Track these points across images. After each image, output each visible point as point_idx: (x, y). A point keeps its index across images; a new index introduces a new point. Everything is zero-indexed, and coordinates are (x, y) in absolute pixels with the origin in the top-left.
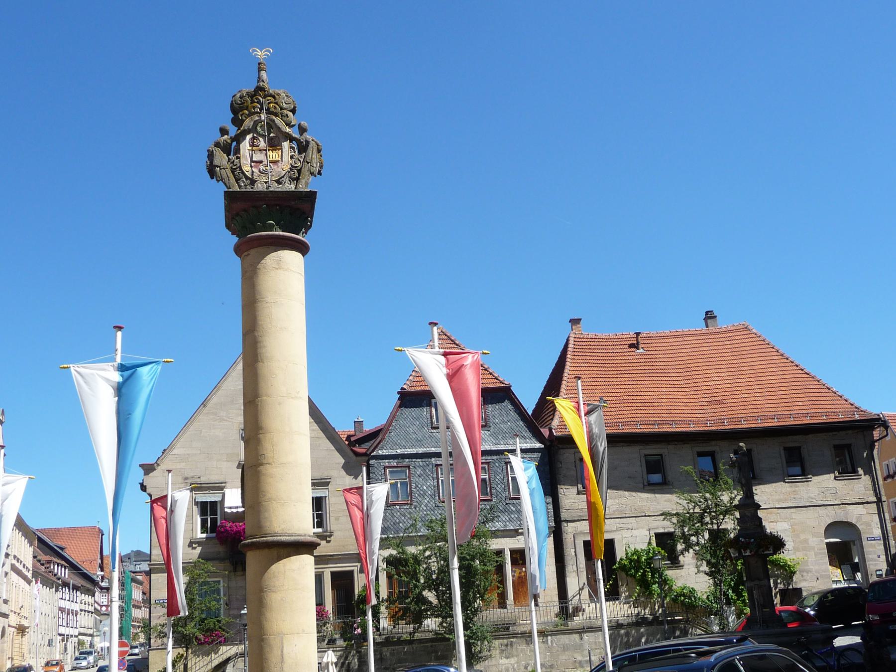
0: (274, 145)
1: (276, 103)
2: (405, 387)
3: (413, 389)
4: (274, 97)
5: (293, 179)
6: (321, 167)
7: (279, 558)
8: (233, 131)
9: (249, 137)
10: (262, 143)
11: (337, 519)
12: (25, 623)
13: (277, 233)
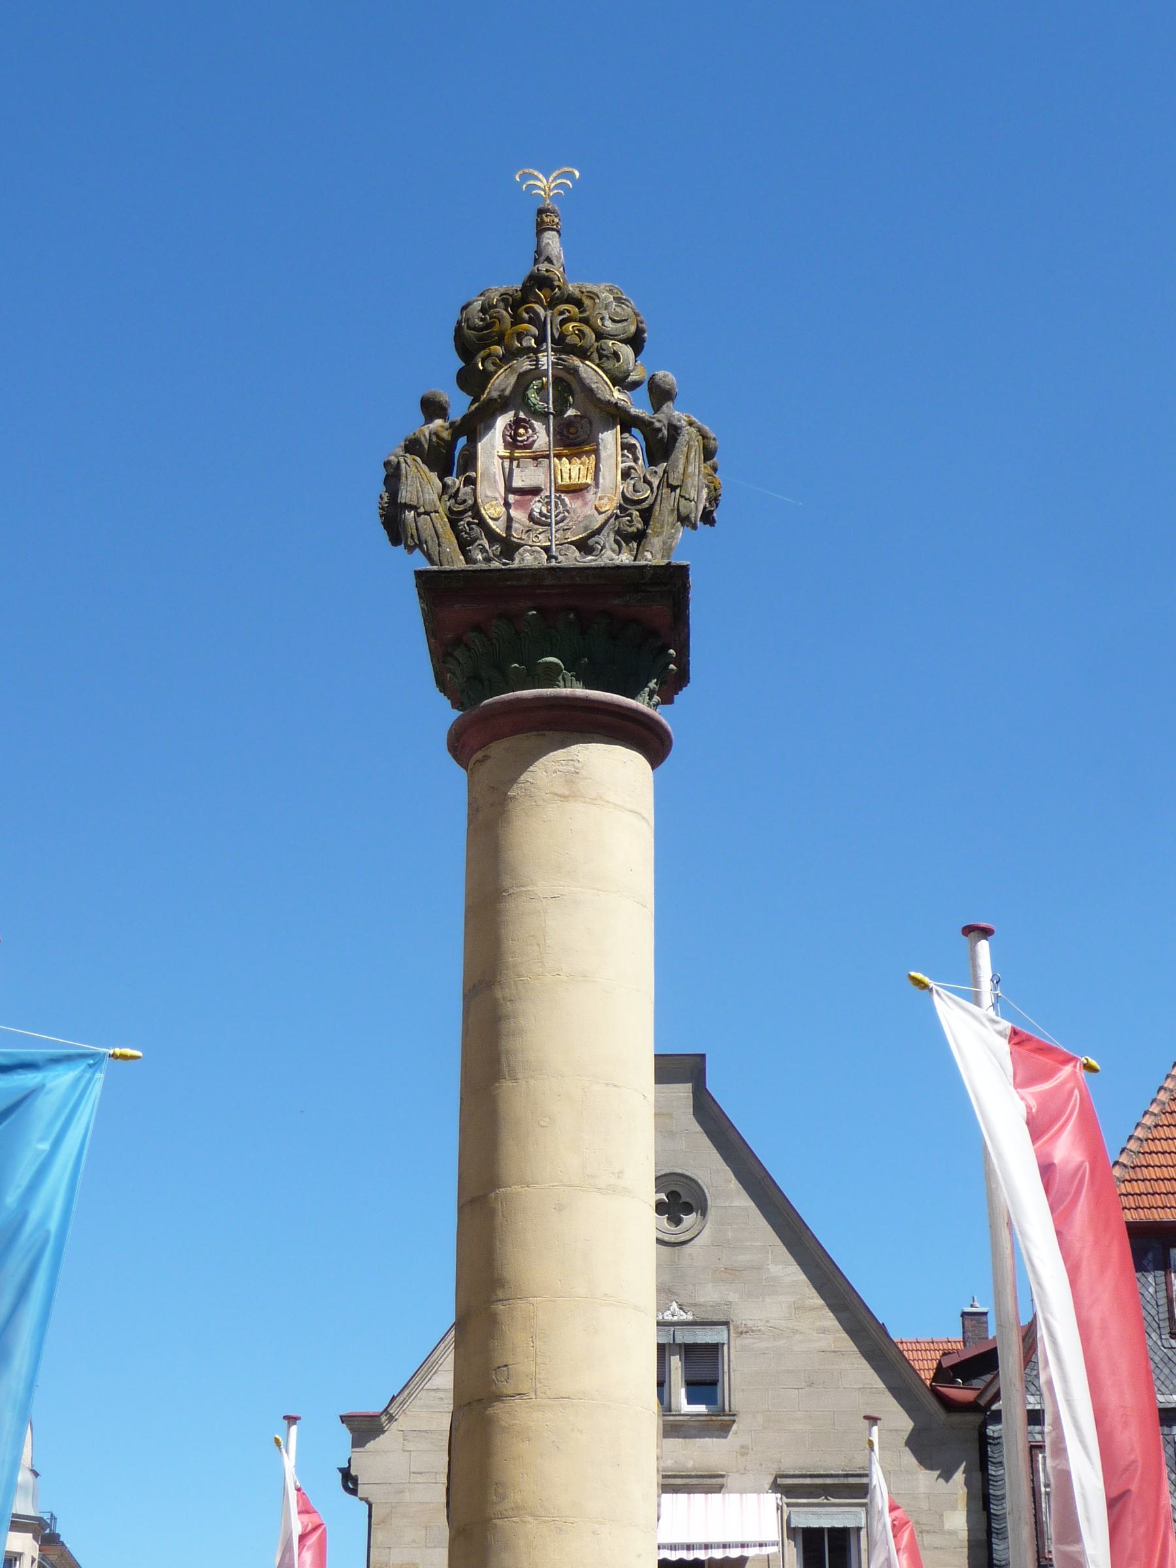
0: (574, 440)
1: (585, 321)
4: (579, 303)
6: (714, 500)
8: (459, 405)
9: (502, 422)
10: (541, 436)
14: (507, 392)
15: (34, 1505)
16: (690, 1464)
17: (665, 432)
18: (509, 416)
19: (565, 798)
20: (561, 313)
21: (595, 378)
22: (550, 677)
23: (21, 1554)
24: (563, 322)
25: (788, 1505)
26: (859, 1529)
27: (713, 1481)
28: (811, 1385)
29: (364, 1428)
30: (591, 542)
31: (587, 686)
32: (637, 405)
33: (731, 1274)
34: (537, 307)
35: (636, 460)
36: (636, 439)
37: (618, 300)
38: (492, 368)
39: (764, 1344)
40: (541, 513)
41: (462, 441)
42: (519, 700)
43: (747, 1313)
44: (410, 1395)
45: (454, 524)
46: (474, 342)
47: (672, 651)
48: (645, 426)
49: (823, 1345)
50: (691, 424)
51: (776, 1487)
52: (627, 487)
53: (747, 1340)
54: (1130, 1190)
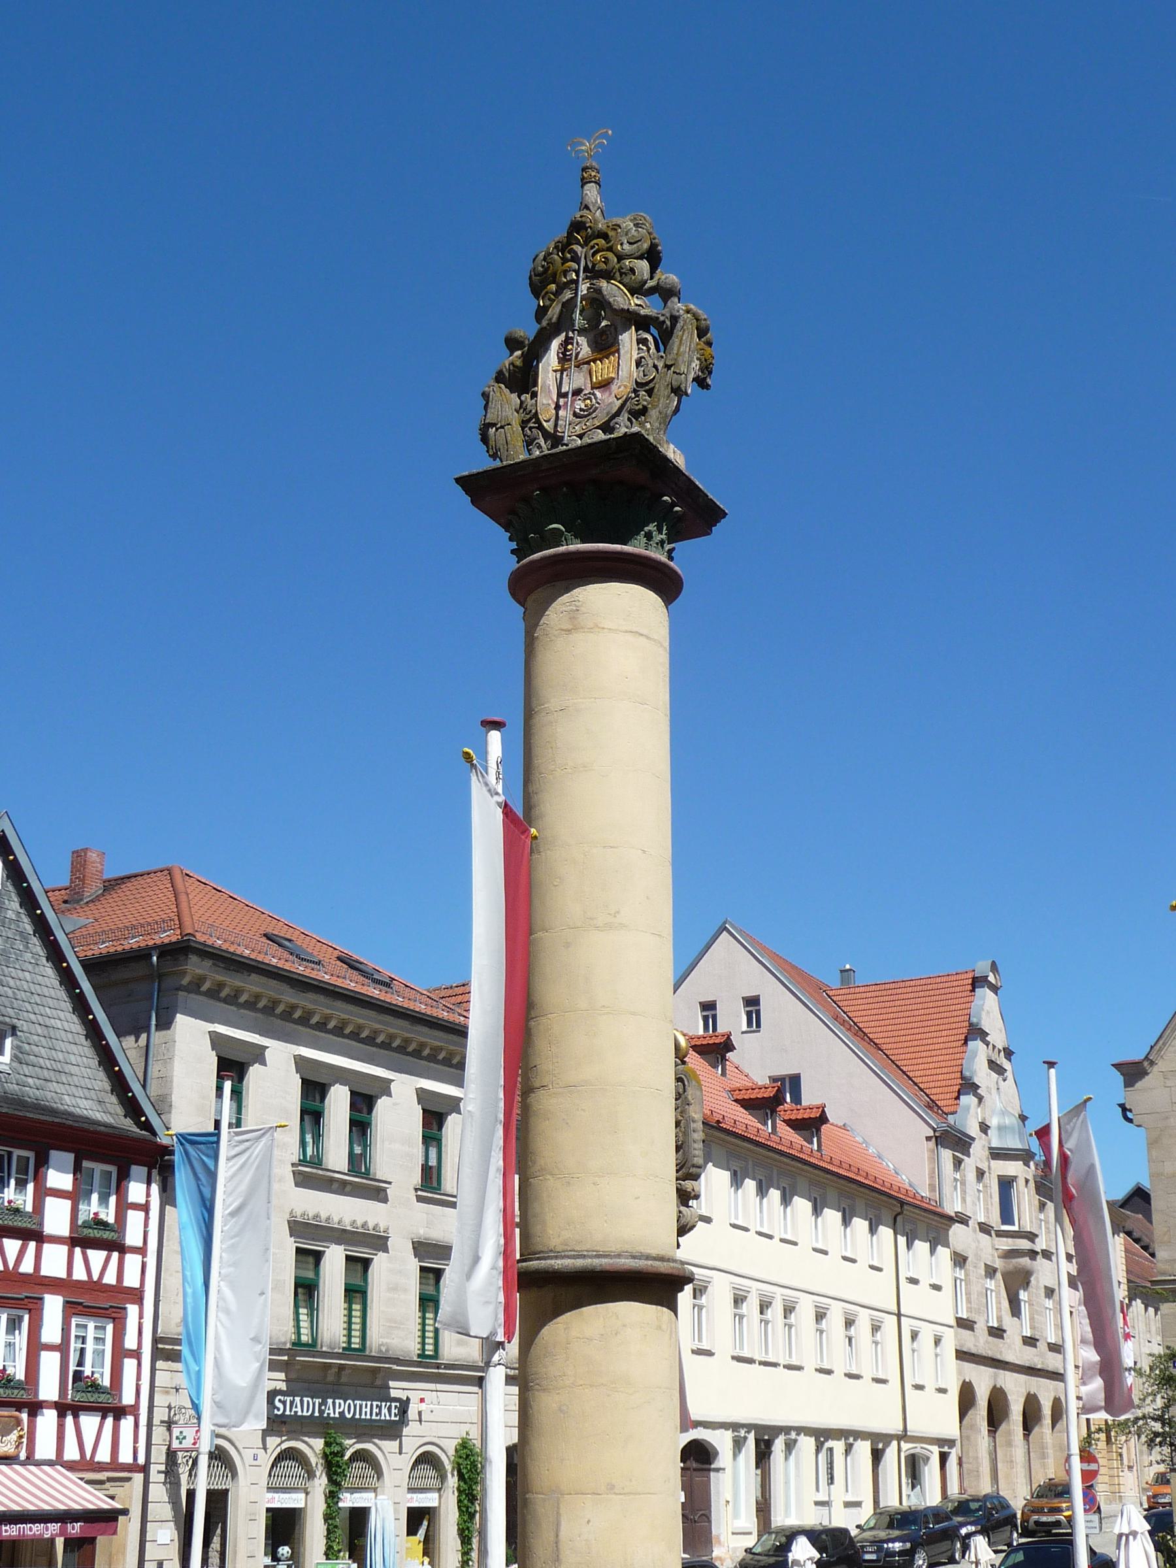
0: (605, 346)
1: (610, 249)
6: (707, 368)
7: (557, 1312)
9: (555, 344)
10: (582, 346)
13: (572, 547)
14: (554, 320)
15: (1021, 1140)
17: (668, 323)
18: (562, 337)
19: (569, 631)
20: (592, 247)
21: (617, 292)
22: (556, 539)
23: (1016, 1177)
24: (594, 255)
29: (1132, 1072)
30: (612, 424)
31: (583, 542)
34: (574, 247)
37: (636, 225)
40: (581, 410)
42: (532, 562)
44: (1164, 1044)
47: (665, 498)
50: (688, 312)
52: (636, 374)
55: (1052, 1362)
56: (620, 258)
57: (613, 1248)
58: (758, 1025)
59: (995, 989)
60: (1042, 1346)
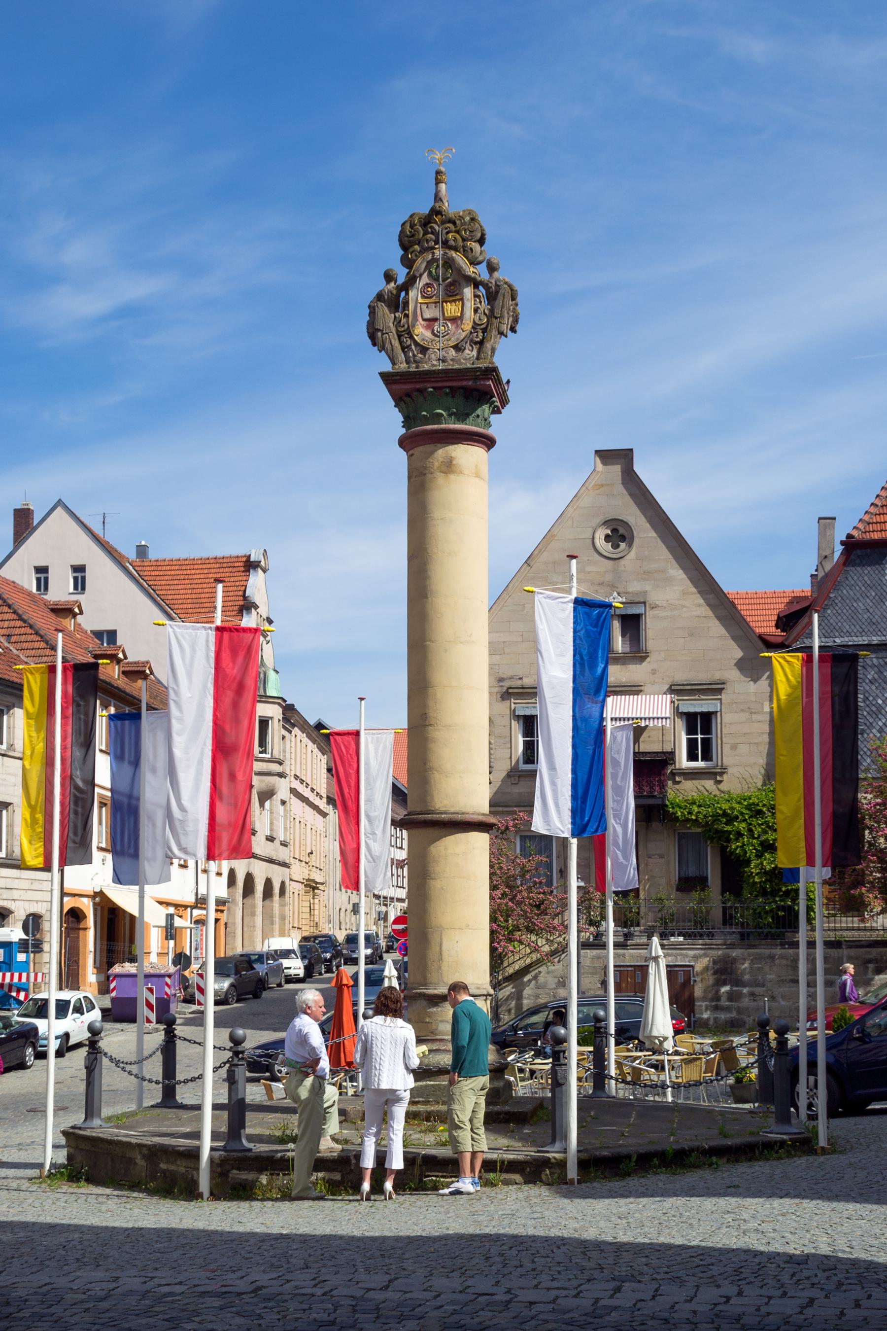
0: (453, 293)
1: (458, 232)
2: (855, 533)
3: (867, 537)
4: (454, 223)
5: (476, 343)
8: (402, 274)
11: (734, 747)
12: (318, 877)
16: (624, 680)
22: (438, 418)
24: (448, 233)
25: (678, 700)
26: (717, 712)
27: (636, 688)
28: (691, 635)
32: (481, 272)
33: (646, 575)
35: (480, 302)
36: (482, 291)
38: (414, 258)
39: (665, 614)
41: (403, 294)
43: (654, 597)
45: (399, 336)
46: (407, 242)
48: (487, 287)
49: (698, 613)
51: (672, 690)
53: (656, 612)
54: (879, 520)
55: (283, 854)
56: (464, 240)
57: (452, 810)
58: (83, 588)
59: (264, 571)
60: (277, 842)
